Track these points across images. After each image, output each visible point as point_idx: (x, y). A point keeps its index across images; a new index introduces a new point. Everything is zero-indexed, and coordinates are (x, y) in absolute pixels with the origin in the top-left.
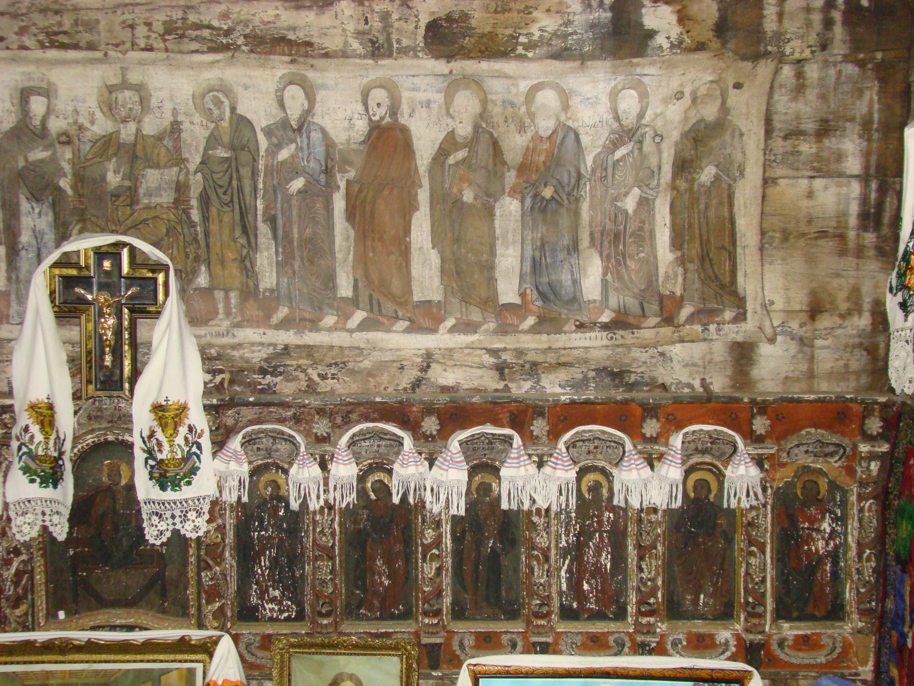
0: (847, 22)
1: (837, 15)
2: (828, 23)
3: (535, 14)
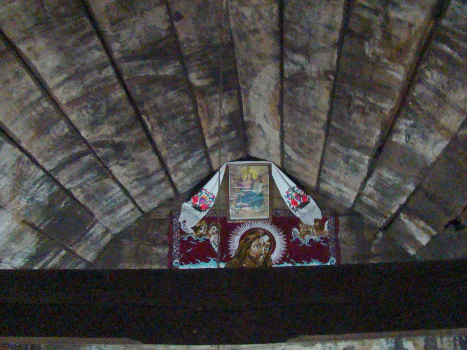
0: (460, 344)
1: (457, 343)
2: (455, 345)
3: (373, 346)
